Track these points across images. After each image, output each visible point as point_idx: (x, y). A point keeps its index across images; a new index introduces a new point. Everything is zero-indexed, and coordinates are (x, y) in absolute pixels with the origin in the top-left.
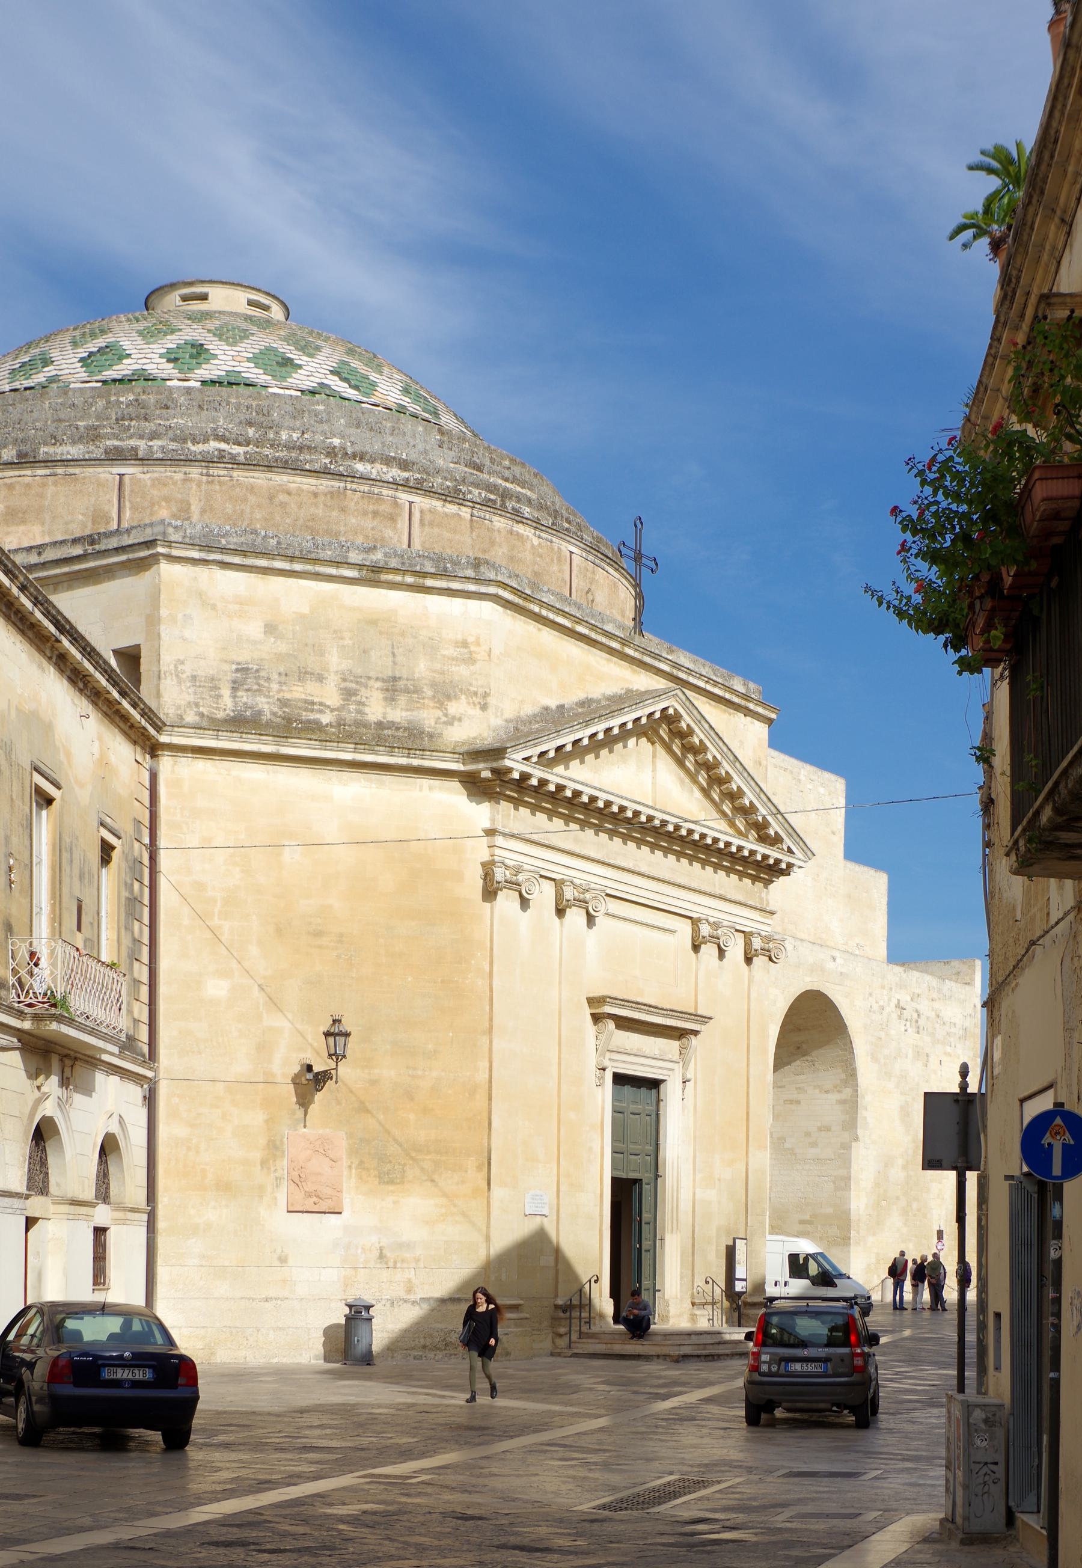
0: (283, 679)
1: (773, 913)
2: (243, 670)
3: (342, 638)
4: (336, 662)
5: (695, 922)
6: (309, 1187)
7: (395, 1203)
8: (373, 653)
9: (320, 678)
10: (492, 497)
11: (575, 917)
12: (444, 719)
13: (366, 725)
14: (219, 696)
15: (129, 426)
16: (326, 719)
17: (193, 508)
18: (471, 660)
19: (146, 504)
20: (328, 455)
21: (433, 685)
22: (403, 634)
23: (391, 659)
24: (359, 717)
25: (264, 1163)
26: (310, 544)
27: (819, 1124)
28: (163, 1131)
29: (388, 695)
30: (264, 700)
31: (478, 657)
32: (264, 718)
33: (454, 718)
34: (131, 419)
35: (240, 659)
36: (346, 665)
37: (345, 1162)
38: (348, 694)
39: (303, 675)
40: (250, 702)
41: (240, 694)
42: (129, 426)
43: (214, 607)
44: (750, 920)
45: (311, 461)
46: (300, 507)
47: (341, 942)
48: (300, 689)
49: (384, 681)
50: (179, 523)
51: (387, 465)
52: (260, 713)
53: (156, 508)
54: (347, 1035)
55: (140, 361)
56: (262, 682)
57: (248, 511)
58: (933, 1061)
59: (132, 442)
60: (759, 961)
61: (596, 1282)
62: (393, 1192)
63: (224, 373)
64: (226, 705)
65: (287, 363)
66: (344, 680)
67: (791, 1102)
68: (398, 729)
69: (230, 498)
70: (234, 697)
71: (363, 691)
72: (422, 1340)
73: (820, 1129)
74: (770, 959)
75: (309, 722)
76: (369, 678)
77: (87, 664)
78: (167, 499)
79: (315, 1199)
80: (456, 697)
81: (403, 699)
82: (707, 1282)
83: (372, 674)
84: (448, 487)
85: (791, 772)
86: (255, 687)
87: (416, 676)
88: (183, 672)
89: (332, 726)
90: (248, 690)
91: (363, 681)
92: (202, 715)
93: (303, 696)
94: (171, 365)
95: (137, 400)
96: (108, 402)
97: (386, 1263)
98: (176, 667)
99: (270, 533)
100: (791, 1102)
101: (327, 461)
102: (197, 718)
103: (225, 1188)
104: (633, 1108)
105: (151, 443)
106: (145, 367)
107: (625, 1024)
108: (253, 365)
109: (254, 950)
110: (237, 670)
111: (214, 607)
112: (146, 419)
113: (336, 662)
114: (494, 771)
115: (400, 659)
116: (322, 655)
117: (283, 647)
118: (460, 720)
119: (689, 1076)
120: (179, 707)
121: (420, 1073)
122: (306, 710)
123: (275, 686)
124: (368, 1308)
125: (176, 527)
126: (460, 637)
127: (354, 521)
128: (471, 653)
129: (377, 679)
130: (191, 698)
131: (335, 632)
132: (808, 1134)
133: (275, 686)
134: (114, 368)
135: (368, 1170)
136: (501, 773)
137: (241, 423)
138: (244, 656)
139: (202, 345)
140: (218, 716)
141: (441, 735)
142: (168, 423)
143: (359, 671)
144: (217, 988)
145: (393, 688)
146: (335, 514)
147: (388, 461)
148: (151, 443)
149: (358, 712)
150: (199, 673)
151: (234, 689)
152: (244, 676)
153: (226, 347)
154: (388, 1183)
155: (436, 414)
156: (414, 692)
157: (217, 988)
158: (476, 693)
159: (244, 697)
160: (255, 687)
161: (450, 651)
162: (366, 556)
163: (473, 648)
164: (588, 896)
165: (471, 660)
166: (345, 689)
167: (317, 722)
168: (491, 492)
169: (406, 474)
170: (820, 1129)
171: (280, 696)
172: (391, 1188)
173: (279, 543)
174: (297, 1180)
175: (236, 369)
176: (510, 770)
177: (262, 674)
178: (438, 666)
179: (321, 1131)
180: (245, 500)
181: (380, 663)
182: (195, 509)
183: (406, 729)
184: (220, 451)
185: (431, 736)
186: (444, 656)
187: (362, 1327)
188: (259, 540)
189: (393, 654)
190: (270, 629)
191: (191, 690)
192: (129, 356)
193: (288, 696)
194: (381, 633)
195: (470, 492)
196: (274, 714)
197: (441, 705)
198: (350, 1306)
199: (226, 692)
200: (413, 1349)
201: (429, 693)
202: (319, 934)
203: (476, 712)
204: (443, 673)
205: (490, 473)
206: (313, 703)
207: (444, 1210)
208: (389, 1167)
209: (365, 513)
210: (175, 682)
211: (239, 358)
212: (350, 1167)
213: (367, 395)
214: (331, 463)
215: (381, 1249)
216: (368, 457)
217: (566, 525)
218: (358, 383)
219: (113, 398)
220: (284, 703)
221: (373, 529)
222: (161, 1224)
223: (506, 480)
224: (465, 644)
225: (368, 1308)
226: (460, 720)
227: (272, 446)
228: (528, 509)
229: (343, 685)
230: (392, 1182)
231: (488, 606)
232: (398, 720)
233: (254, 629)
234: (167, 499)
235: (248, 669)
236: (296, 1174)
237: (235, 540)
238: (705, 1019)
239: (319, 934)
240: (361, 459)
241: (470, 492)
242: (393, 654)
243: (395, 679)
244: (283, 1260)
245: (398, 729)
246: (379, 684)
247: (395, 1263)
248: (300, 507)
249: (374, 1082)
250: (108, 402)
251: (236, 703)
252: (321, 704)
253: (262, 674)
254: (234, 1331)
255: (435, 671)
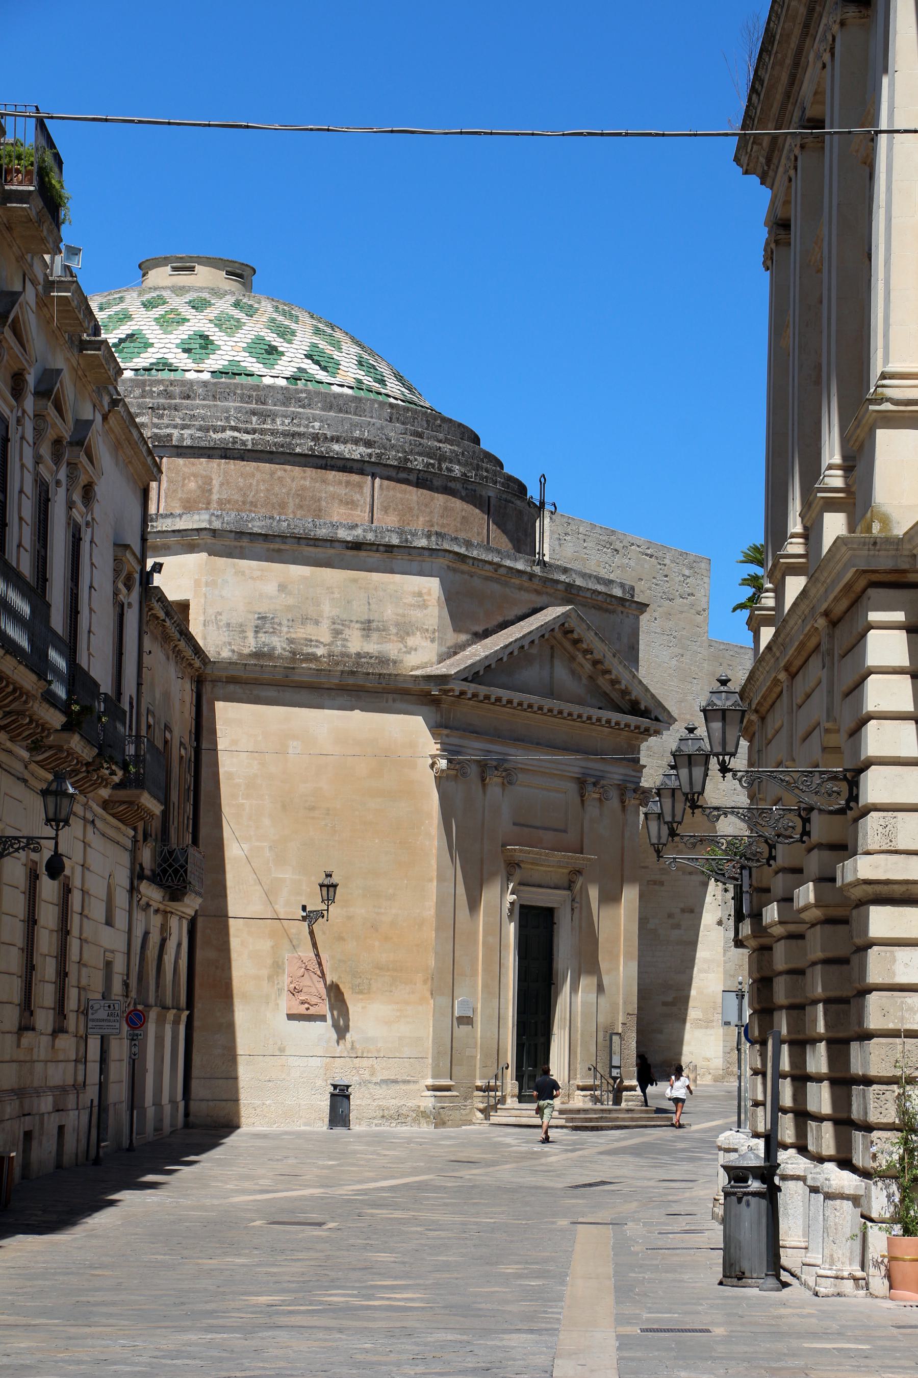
0: (290, 624)
2: (263, 618)
3: (333, 593)
4: (328, 610)
7: (363, 1008)
8: (354, 603)
9: (317, 623)
10: (432, 461)
12: (404, 649)
13: (349, 656)
14: (245, 638)
15: (163, 414)
17: (214, 482)
19: (180, 479)
20: (313, 439)
21: (397, 625)
22: (376, 589)
23: (367, 607)
24: (344, 649)
25: (270, 978)
26: (311, 525)
27: (682, 905)
28: (199, 955)
29: (364, 633)
31: (429, 603)
32: (277, 652)
33: (411, 648)
34: (165, 409)
35: (260, 610)
36: (335, 612)
38: (337, 633)
39: (305, 620)
40: (267, 641)
41: (260, 635)
42: (163, 414)
45: (300, 445)
46: (293, 480)
47: (328, 814)
48: (302, 631)
49: (362, 623)
50: (219, 513)
51: (356, 444)
52: (274, 649)
53: (186, 481)
55: (161, 350)
56: (276, 626)
57: (255, 483)
59: (168, 431)
62: (362, 999)
63: (227, 363)
65: (272, 350)
66: (334, 623)
67: (655, 883)
68: (371, 657)
69: (242, 475)
70: (256, 638)
71: (347, 631)
73: (683, 911)
75: (308, 654)
76: (351, 621)
78: (195, 475)
80: (414, 634)
81: (375, 636)
84: (400, 458)
85: (657, 558)
86: (271, 630)
89: (324, 657)
90: (265, 632)
92: (233, 651)
93: (305, 636)
94: (186, 355)
95: (166, 390)
96: (144, 391)
98: (216, 617)
99: (283, 517)
100: (655, 883)
101: (312, 444)
102: (230, 654)
105: (182, 432)
106: (166, 356)
108: (247, 354)
109: (267, 822)
110: (259, 618)
112: (176, 410)
115: (373, 606)
116: (318, 606)
117: (291, 601)
118: (416, 650)
120: (217, 646)
121: (383, 910)
122: (306, 645)
123: (285, 629)
124: (348, 1086)
125: (217, 516)
126: (416, 589)
127: (332, 489)
128: (424, 600)
129: (357, 622)
130: (227, 639)
131: (328, 588)
132: (670, 916)
133: (285, 629)
134: (142, 355)
137: (247, 412)
138: (263, 608)
139: (208, 336)
140: (245, 652)
141: (401, 662)
142: (192, 413)
143: (344, 617)
145: (368, 627)
146: (317, 484)
147: (356, 441)
148: (182, 432)
149: (343, 646)
150: (233, 621)
151: (256, 632)
153: (226, 338)
155: (382, 382)
156: (383, 630)
158: (427, 630)
159: (263, 638)
160: (271, 630)
161: (410, 600)
162: (350, 532)
163: (426, 597)
166: (334, 629)
168: (431, 458)
169: (369, 451)
170: (683, 911)
171: (288, 636)
172: (361, 996)
173: (288, 525)
175: (236, 359)
177: (276, 620)
178: (401, 611)
180: (253, 475)
182: (216, 483)
183: (377, 658)
184: (234, 438)
185: (395, 662)
186: (405, 604)
188: (275, 523)
189: (369, 603)
191: (226, 634)
192: (152, 345)
193: (293, 636)
194: (360, 588)
195: (416, 460)
196: (284, 649)
197: (402, 640)
199: (250, 634)
200: (374, 1118)
201: (393, 630)
202: (312, 809)
205: (428, 438)
206: (311, 641)
208: (359, 980)
209: (340, 483)
210: (215, 628)
211: (237, 349)
213: (334, 375)
214: (315, 445)
216: (342, 439)
217: (485, 474)
218: (327, 364)
219: (148, 388)
220: (291, 641)
221: (345, 494)
223: (440, 441)
225: (348, 1086)
226: (416, 650)
227: (272, 434)
228: (457, 467)
230: (361, 992)
232: (371, 651)
234: (195, 475)
235: (266, 617)
237: (258, 524)
239: (312, 809)
240: (337, 442)
241: (416, 460)
242: (369, 603)
243: (369, 621)
245: (371, 657)
246: (358, 626)
248: (293, 480)
249: (350, 918)
250: (144, 391)
251: (257, 642)
252: (317, 641)
253: (276, 620)
255: (398, 615)
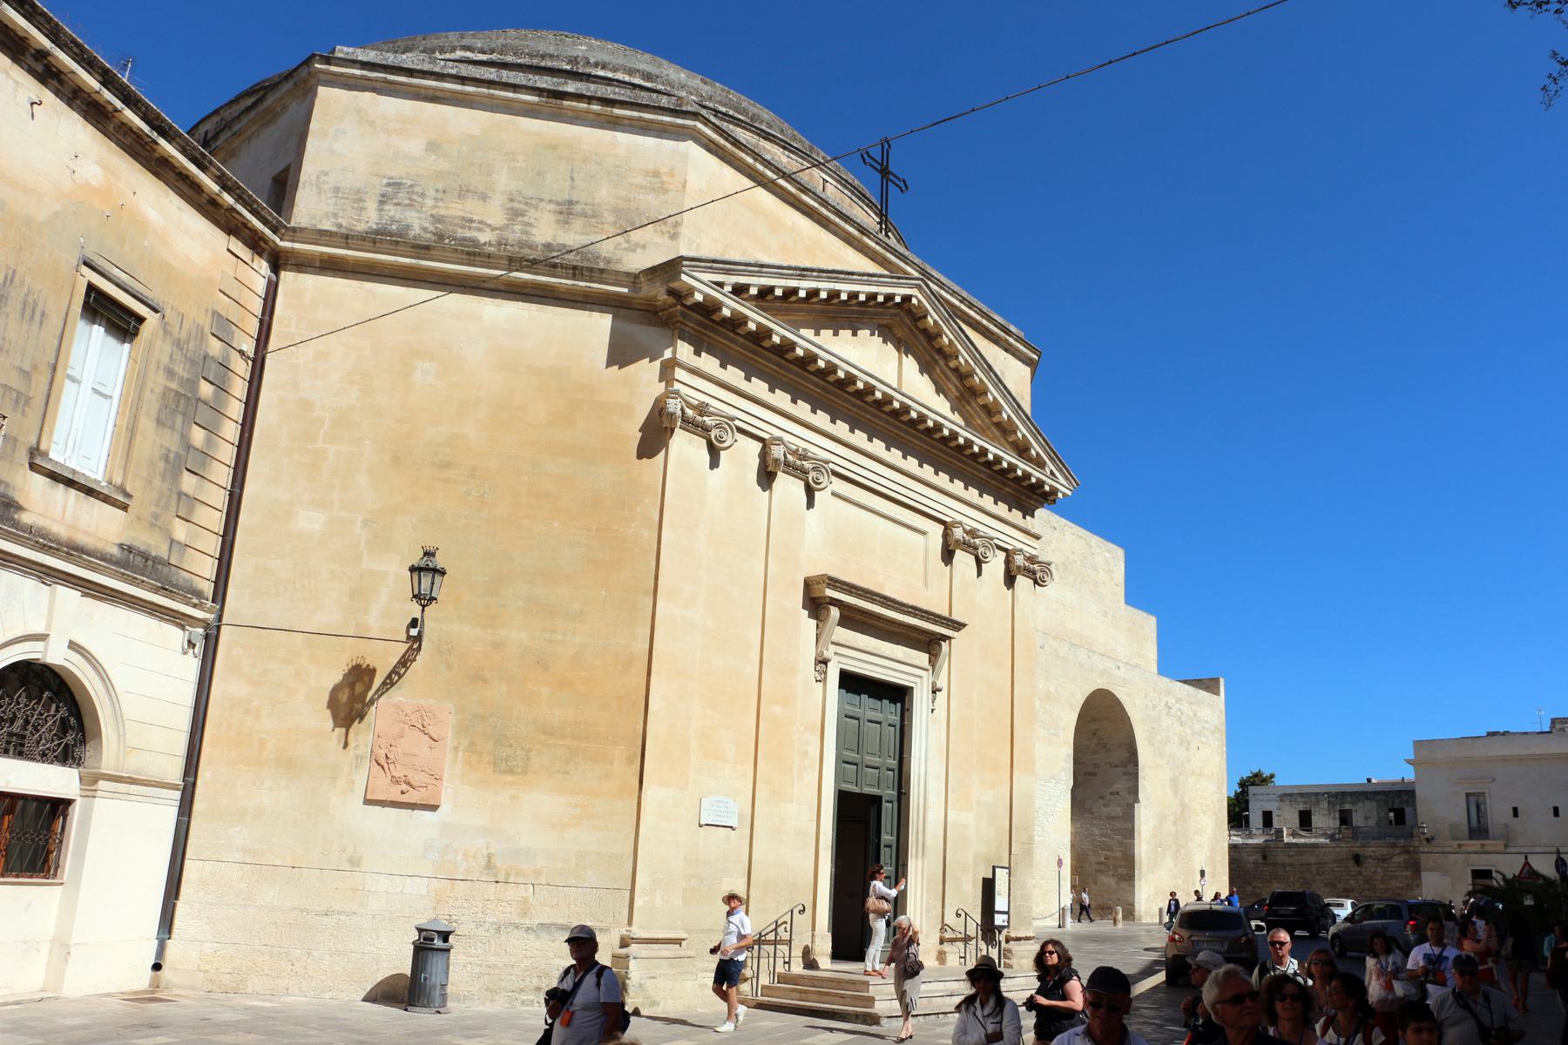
0: (440, 195)
1: (1038, 538)
4: (504, 181)
5: (947, 527)
6: (399, 772)
7: (513, 798)
9: (484, 197)
11: (788, 487)
12: (625, 245)
16: (483, 237)
18: (664, 190)
21: (616, 211)
22: (585, 160)
23: (568, 183)
24: (525, 237)
29: (562, 217)
30: (414, 214)
32: (412, 233)
33: (637, 245)
35: (393, 174)
37: (450, 742)
38: (515, 214)
39: (464, 192)
40: (398, 216)
41: (387, 207)
43: (372, 124)
44: (1014, 539)
49: (558, 203)
54: (443, 573)
58: (1193, 747)
60: (1022, 582)
61: (802, 911)
62: (511, 784)
64: (370, 218)
71: (532, 213)
72: (535, 980)
74: (1036, 582)
75: (464, 239)
77: (107, 95)
79: (404, 787)
81: (578, 223)
82: (958, 915)
83: (546, 196)
87: (597, 201)
88: (325, 183)
91: (533, 202)
97: (495, 875)
103: (288, 764)
104: (871, 715)
107: (855, 619)
110: (389, 184)
111: (372, 124)
113: (504, 181)
114: (671, 292)
117: (444, 165)
118: (644, 247)
119: (939, 685)
120: (314, 217)
121: (559, 637)
122: (463, 227)
124: (445, 936)
126: (651, 167)
130: (331, 209)
131: (507, 154)
135: (480, 754)
136: (679, 295)
138: (398, 171)
143: (530, 193)
144: (310, 521)
145: (566, 211)
151: (382, 203)
152: (393, 191)
154: (505, 772)
157: (310, 521)
159: (391, 211)
161: (640, 180)
164: (807, 465)
165: (664, 190)
167: (474, 242)
172: (509, 778)
174: (383, 761)
176: (691, 291)
178: (624, 193)
179: (422, 702)
181: (555, 185)
187: (435, 961)
190: (432, 147)
193: (442, 212)
194: (560, 158)
196: (425, 230)
198: (420, 930)
199: (371, 206)
202: (445, 466)
203: (666, 240)
204: (628, 200)
206: (471, 221)
207: (578, 811)
208: (508, 751)
212: (456, 749)
215: (489, 857)
220: (437, 219)
222: (198, 806)
224: (656, 174)
225: (445, 936)
226: (644, 247)
229: (510, 205)
230: (511, 771)
231: (691, 147)
233: (415, 146)
236: (382, 753)
238: (958, 626)
239: (445, 466)
243: (571, 203)
244: (355, 862)
246: (552, 207)
247: (508, 875)
251: (381, 217)
252: (480, 222)
254: (276, 950)
